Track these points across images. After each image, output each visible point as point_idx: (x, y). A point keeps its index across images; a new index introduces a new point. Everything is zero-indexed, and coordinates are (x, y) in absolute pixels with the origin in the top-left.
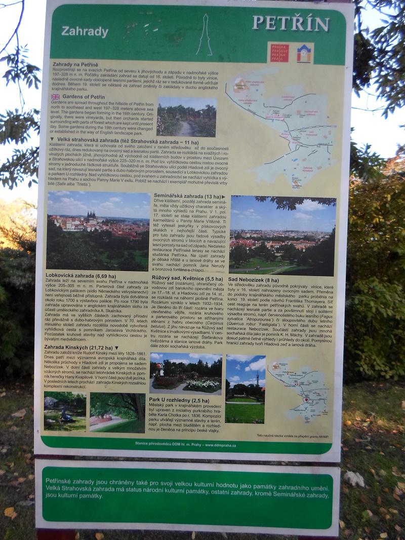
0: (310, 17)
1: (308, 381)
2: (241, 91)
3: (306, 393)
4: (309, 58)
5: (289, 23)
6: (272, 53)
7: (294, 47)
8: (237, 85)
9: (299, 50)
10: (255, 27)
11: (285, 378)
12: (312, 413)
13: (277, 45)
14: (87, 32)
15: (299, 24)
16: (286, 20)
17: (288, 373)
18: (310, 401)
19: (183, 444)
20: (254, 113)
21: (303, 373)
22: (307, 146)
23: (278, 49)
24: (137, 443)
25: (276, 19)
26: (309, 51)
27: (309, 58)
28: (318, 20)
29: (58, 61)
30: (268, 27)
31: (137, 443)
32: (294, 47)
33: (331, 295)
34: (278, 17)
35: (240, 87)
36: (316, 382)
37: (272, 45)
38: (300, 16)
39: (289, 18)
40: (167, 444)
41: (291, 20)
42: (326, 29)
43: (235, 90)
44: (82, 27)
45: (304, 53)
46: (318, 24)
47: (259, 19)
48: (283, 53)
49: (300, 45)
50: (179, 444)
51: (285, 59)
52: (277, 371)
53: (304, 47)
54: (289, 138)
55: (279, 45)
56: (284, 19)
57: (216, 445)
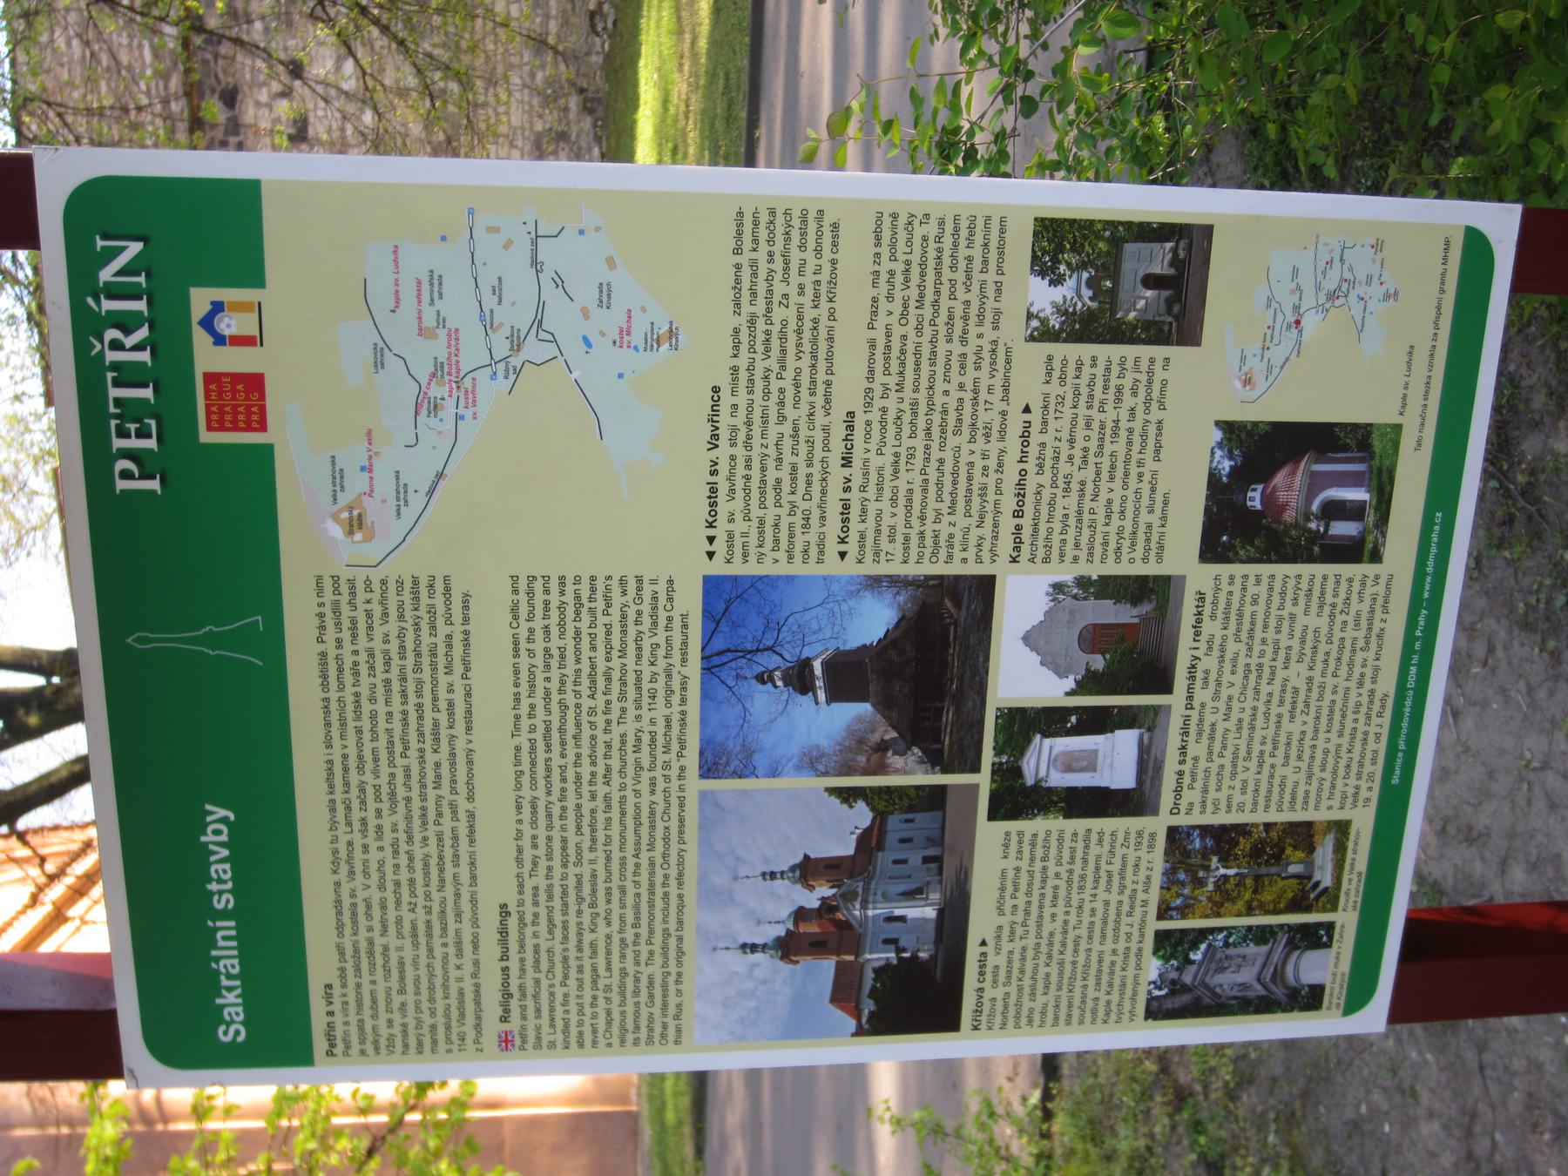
0: (98, 301)
1: (1293, 292)
2: (368, 520)
3: (1322, 299)
4: (243, 307)
5: (128, 376)
6: (235, 429)
7: (208, 358)
8: (351, 533)
9: (219, 340)
10: (154, 485)
11: (1277, 355)
12: (1375, 282)
13: (209, 413)
14: (229, 976)
15: (130, 341)
16: (117, 383)
17: (1265, 348)
18: (1345, 287)
19: (1415, 659)
20: (440, 476)
21: (1269, 306)
22: (541, 306)
23: (221, 407)
24: (1395, 780)
25: (117, 416)
26: (218, 307)
27: (243, 307)
28: (106, 275)
29: (319, 1044)
30: (151, 444)
31: (1395, 780)
32: (208, 358)
33: (559, 1043)
34: (112, 410)
35: (355, 524)
36: (1295, 271)
37: (210, 428)
38: (102, 341)
39: (110, 375)
40: (1408, 703)
41: (116, 366)
42: (135, 248)
43: (368, 538)
44: (217, 990)
45: (228, 325)
46: (119, 273)
47: (126, 475)
48: (234, 391)
49: (201, 338)
50: (1413, 670)
51: (254, 383)
52: (1259, 378)
53: (208, 323)
54: (516, 362)
55: (208, 407)
56: (114, 393)
57: (1429, 570)
